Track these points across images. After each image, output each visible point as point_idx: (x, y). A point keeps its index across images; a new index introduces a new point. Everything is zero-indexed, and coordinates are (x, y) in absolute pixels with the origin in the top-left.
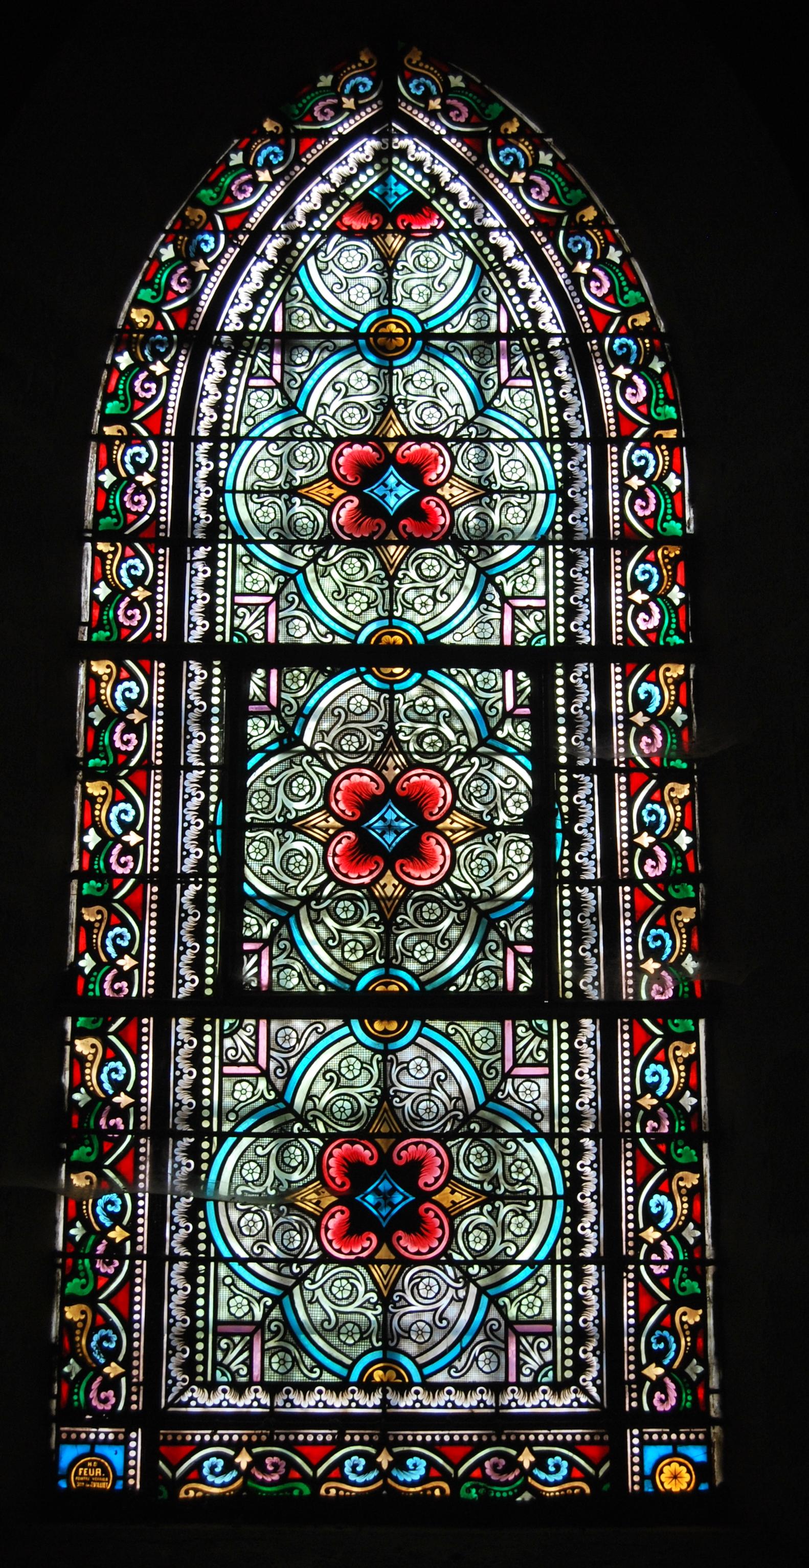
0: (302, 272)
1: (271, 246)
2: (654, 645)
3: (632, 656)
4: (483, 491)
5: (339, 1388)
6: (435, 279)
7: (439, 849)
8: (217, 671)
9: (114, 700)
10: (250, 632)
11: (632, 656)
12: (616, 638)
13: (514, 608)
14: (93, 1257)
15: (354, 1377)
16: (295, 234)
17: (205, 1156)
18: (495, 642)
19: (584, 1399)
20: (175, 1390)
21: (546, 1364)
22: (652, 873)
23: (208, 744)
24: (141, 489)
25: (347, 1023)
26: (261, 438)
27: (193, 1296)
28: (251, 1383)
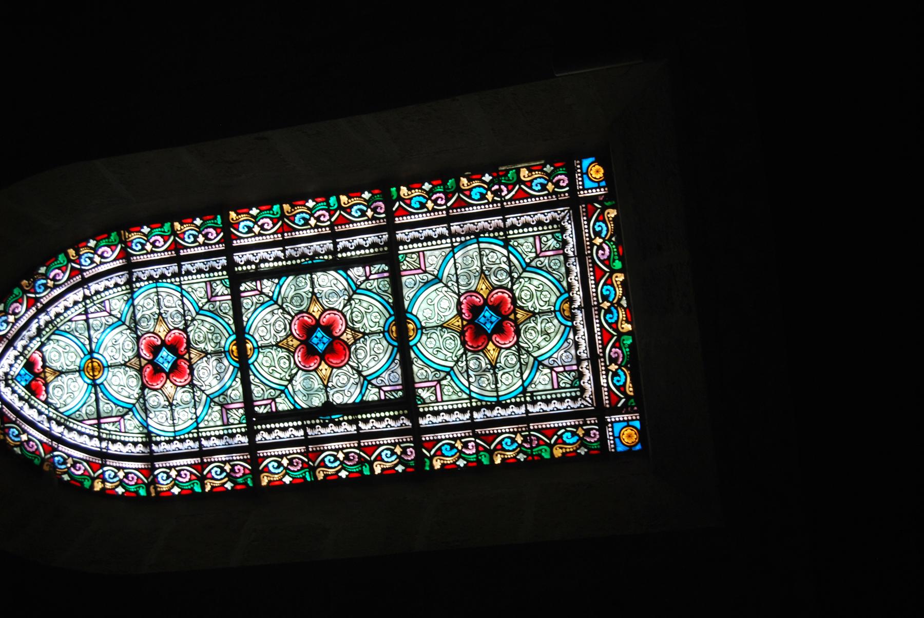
0: (67, 414)
1: (57, 430)
2: (223, 229)
3: (228, 238)
4: (160, 317)
5: (575, 330)
6: (62, 353)
7: (497, 294)
8: (259, 427)
9: (574, 444)
10: (572, 378)
11: (228, 238)
12: (221, 247)
13: (212, 296)
14: (532, 448)
15: (569, 324)
16: (50, 419)
17: (479, 403)
18: (230, 302)
19: (567, 218)
20: (586, 403)
21: (553, 237)
22: (328, 218)
23: (293, 427)
24: (233, 470)
25: (411, 347)
26: (469, 388)
27: (557, 399)
28: (578, 370)
